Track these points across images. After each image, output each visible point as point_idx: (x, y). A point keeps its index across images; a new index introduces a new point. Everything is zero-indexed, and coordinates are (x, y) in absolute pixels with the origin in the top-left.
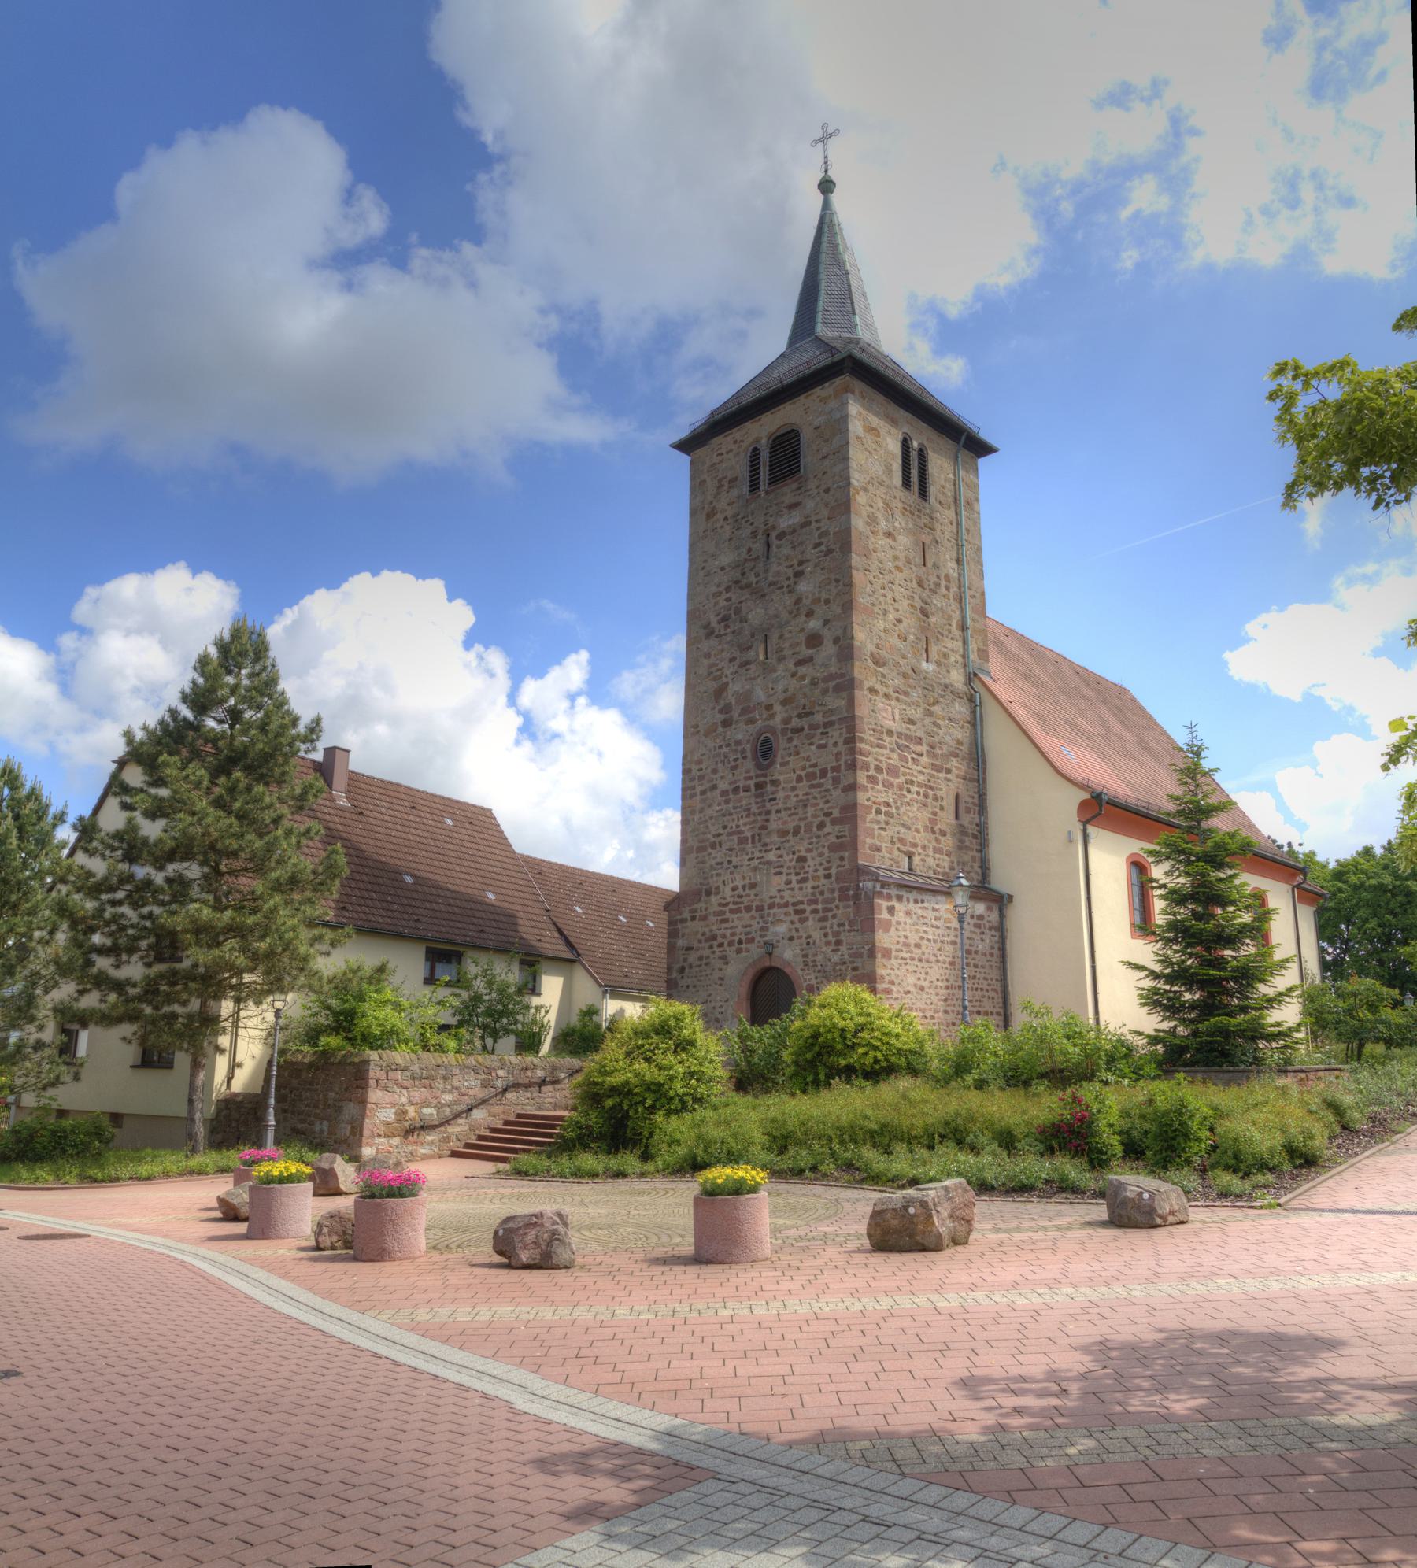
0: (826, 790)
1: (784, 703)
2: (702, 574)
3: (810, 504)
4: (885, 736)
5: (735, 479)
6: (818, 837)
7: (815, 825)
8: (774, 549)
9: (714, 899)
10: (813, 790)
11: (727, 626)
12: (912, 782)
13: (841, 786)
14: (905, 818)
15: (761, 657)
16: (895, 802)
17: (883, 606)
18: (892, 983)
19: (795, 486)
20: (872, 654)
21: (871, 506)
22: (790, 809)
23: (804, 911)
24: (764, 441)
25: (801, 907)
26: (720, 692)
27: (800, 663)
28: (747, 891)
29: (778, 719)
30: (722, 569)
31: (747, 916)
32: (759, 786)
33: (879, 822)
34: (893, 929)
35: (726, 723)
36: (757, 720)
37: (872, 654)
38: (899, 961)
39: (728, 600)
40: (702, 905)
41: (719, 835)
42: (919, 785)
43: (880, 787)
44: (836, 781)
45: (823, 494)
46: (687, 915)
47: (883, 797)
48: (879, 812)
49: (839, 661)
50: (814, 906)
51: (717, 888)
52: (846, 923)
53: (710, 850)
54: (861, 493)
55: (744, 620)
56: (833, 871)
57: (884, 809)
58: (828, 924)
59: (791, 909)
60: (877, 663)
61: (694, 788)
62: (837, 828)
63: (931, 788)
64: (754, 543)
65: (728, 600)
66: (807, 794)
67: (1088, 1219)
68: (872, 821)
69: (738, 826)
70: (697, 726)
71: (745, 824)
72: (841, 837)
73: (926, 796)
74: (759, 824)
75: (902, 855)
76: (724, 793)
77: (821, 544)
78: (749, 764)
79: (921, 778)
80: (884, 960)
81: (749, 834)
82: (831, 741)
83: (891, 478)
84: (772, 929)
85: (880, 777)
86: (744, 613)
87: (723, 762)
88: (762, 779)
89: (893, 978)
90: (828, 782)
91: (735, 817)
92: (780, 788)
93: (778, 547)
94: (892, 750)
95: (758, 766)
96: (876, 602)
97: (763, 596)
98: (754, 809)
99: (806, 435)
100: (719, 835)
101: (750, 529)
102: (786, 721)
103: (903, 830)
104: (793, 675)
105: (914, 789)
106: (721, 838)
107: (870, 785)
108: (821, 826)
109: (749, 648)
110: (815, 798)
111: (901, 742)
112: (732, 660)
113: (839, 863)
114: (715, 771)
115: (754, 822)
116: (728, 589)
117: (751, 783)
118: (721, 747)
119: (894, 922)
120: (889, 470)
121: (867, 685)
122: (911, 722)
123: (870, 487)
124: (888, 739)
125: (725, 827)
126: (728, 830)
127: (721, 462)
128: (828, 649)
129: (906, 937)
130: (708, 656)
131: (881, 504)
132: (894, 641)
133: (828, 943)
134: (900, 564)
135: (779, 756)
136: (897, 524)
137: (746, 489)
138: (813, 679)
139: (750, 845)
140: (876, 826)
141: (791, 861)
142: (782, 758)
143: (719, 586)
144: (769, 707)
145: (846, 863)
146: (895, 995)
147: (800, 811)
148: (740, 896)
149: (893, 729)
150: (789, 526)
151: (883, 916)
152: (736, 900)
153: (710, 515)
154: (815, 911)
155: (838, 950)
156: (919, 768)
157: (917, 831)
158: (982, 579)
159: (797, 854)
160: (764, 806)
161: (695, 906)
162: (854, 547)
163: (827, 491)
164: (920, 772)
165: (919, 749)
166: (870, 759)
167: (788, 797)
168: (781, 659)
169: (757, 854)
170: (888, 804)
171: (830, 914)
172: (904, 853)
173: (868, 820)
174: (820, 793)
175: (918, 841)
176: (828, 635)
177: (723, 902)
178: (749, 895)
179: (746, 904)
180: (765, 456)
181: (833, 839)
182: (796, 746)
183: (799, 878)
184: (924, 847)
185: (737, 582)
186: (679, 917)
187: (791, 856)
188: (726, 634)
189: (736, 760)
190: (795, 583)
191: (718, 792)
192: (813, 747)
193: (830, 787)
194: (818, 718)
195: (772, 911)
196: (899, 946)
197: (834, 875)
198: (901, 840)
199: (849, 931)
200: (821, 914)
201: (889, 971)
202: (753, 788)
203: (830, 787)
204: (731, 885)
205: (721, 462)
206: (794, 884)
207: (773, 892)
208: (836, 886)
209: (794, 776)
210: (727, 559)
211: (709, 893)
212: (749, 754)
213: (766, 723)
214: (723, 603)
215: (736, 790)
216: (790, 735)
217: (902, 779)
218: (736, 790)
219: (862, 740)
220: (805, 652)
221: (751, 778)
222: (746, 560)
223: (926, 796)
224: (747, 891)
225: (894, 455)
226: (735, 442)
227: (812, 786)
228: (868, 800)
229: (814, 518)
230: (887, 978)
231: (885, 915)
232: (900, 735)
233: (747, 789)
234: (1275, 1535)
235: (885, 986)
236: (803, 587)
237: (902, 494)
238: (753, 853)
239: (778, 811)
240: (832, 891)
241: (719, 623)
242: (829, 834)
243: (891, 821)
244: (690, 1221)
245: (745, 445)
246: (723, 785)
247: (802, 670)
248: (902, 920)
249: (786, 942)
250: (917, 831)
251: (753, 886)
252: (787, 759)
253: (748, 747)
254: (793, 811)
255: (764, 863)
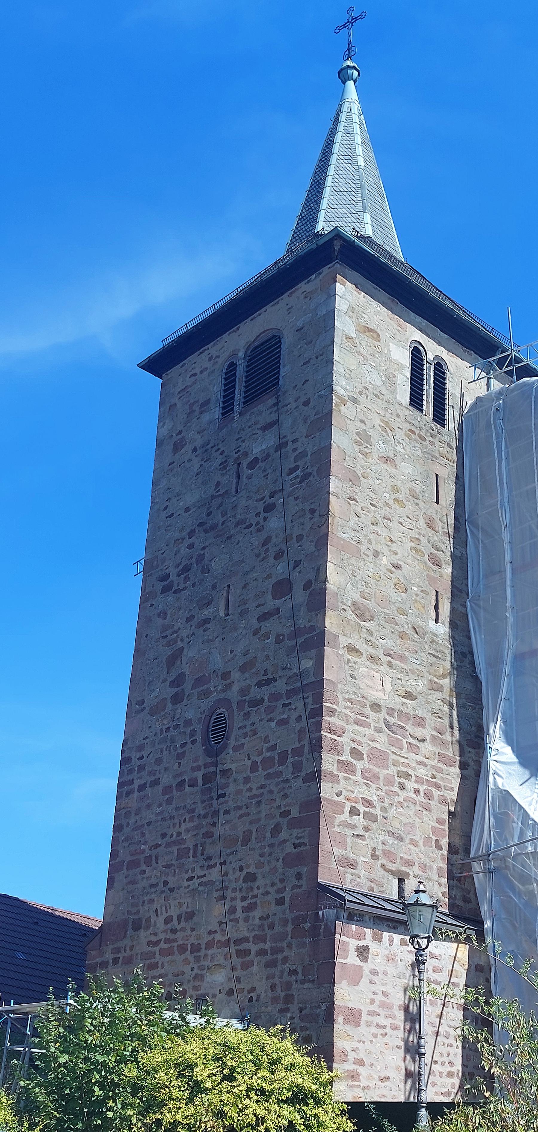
0: (287, 781)
1: (243, 669)
2: (164, 514)
3: (287, 422)
4: (367, 710)
5: (208, 402)
6: (271, 846)
7: (269, 829)
8: (244, 480)
9: (144, 935)
10: (268, 782)
11: (187, 579)
12: (408, 776)
13: (303, 774)
14: (396, 824)
15: (222, 614)
16: (381, 800)
17: (373, 546)
18: (361, 1063)
19: (272, 401)
20: (354, 604)
21: (362, 421)
22: (240, 808)
23: (248, 952)
24: (241, 354)
25: (245, 946)
26: (173, 660)
27: (264, 617)
28: (183, 924)
29: (236, 688)
30: (187, 510)
31: (179, 958)
32: (206, 779)
33: (354, 827)
34: (364, 980)
35: (177, 699)
36: (211, 692)
37: (354, 604)
38: (374, 1030)
39: (191, 546)
40: (127, 942)
41: (157, 846)
42: (419, 780)
43: (358, 777)
44: (297, 767)
45: (301, 407)
46: (109, 956)
47: (361, 792)
48: (354, 812)
49: (309, 611)
50: (261, 945)
51: (149, 920)
52: (300, 970)
53: (144, 867)
54: (349, 404)
55: (206, 570)
56: (287, 895)
57: (362, 809)
58: (277, 971)
59: (233, 949)
60: (361, 616)
61: (132, 782)
62: (295, 832)
63: (437, 786)
64: (223, 475)
65: (191, 546)
66: (263, 787)
67: (302, 330)
68: (344, 824)
69: (179, 834)
70: (143, 702)
71: (187, 831)
72: (299, 845)
73: (428, 796)
74: (204, 830)
75: (391, 877)
76: (167, 790)
77: (296, 468)
78: (199, 749)
79: (422, 772)
80: (348, 1027)
81: (190, 844)
82: (294, 715)
83: (393, 392)
84: (208, 978)
85: (359, 765)
86: (206, 561)
87: (168, 748)
88: (212, 769)
89: (362, 1055)
90: (287, 771)
91: (176, 821)
92: (231, 779)
93: (249, 477)
94: (379, 730)
95: (208, 753)
96: (364, 541)
97: (229, 538)
98: (200, 810)
99: (288, 340)
100: (157, 846)
101: (220, 460)
102: (244, 691)
103: (391, 840)
104: (256, 633)
105: (411, 785)
106: (158, 850)
107: (342, 775)
108: (276, 830)
109: (209, 603)
110: (271, 792)
111: (392, 720)
112: (189, 620)
113: (295, 882)
114: (159, 761)
115: (198, 827)
116: (191, 534)
117: (199, 775)
118: (168, 729)
119: (366, 971)
120: (390, 380)
121: (343, 641)
122: (409, 695)
123: (362, 399)
124: (373, 715)
125: (164, 835)
126: (168, 838)
127: (194, 383)
128: (300, 596)
129: (385, 994)
130: (163, 614)
131: (377, 422)
132: (388, 588)
133: (275, 1000)
134: (401, 497)
135: (233, 738)
136: (399, 448)
137: (216, 412)
138: (278, 636)
139: (191, 859)
140: (349, 832)
141: (237, 880)
142: (236, 740)
143: (181, 531)
144: (226, 675)
145: (303, 882)
146: (363, 1083)
147: (253, 810)
148: (174, 931)
149: (382, 703)
150: (263, 451)
151: (348, 961)
152: (170, 936)
153: (177, 447)
154: (262, 952)
155: (287, 1010)
156: (419, 758)
157: (414, 843)
158: (536, 922)
159: (245, 871)
160: (211, 805)
161: (119, 944)
162: (334, 468)
163: (306, 403)
164: (420, 763)
165: (419, 732)
166: (343, 740)
167: (239, 792)
168: (242, 614)
169: (199, 872)
170: (368, 803)
171: (280, 956)
172: (392, 872)
173: (337, 822)
174: (277, 784)
175: (413, 857)
176: (298, 579)
177: (153, 939)
178: (183, 930)
179: (180, 942)
180: (241, 369)
181: (289, 848)
182: (253, 724)
183: (245, 904)
184: (424, 867)
185: (201, 525)
186: (99, 960)
187: (238, 873)
188: (184, 589)
189: (183, 745)
190: (265, 519)
191: (160, 787)
192: (273, 724)
193: (290, 776)
194: (281, 686)
195: (210, 952)
196: (374, 1008)
197: (287, 899)
198: (387, 854)
199: (303, 982)
200: (269, 957)
201: (357, 1045)
202: (200, 782)
203: (290, 776)
204: (165, 915)
205: (194, 383)
206: (239, 914)
207: (214, 925)
208: (289, 916)
209: (249, 763)
210: (191, 499)
211: (137, 926)
212: (199, 737)
213: (223, 695)
214: (184, 551)
215: (181, 784)
216: (247, 709)
217: (392, 771)
218: (181, 784)
219: (332, 712)
220: (271, 603)
221: (198, 768)
222: (213, 497)
223: (428, 796)
224: (183, 924)
225: (400, 367)
226: (210, 359)
227: (268, 776)
228: (338, 794)
229: (290, 438)
230: (352, 1056)
231: (352, 959)
232: (391, 711)
233: (193, 784)
234: (524, 382)
235: (349, 1066)
236: (274, 523)
237: (407, 412)
238: (193, 870)
239: (227, 812)
240: (285, 922)
241: (179, 575)
242: (285, 841)
243: (374, 826)
244: (334, 1039)
245: (220, 360)
246: (166, 779)
247: (266, 626)
248: (380, 969)
249: (223, 996)
250: (414, 843)
251: (190, 916)
252: (243, 741)
253: (199, 728)
254: (244, 810)
255: (205, 884)
